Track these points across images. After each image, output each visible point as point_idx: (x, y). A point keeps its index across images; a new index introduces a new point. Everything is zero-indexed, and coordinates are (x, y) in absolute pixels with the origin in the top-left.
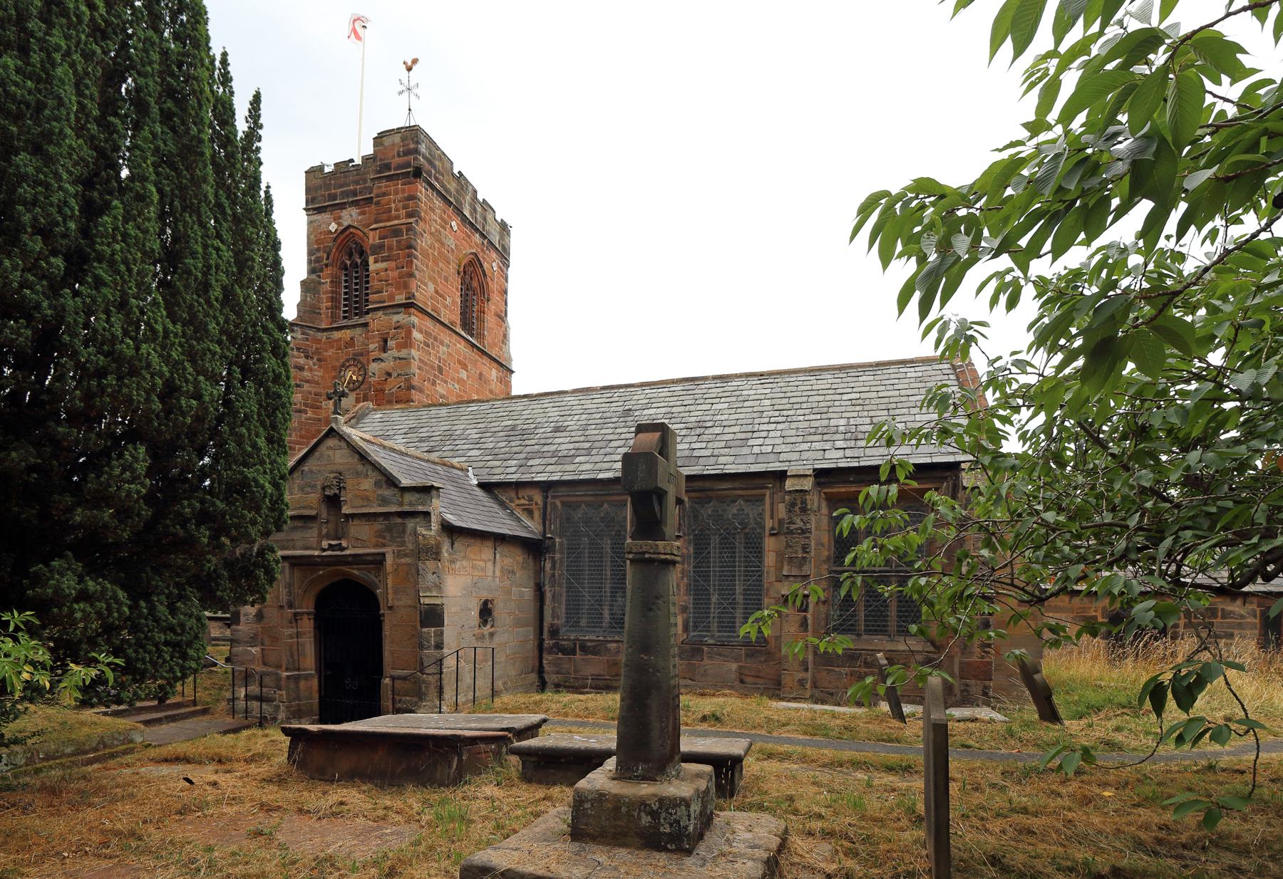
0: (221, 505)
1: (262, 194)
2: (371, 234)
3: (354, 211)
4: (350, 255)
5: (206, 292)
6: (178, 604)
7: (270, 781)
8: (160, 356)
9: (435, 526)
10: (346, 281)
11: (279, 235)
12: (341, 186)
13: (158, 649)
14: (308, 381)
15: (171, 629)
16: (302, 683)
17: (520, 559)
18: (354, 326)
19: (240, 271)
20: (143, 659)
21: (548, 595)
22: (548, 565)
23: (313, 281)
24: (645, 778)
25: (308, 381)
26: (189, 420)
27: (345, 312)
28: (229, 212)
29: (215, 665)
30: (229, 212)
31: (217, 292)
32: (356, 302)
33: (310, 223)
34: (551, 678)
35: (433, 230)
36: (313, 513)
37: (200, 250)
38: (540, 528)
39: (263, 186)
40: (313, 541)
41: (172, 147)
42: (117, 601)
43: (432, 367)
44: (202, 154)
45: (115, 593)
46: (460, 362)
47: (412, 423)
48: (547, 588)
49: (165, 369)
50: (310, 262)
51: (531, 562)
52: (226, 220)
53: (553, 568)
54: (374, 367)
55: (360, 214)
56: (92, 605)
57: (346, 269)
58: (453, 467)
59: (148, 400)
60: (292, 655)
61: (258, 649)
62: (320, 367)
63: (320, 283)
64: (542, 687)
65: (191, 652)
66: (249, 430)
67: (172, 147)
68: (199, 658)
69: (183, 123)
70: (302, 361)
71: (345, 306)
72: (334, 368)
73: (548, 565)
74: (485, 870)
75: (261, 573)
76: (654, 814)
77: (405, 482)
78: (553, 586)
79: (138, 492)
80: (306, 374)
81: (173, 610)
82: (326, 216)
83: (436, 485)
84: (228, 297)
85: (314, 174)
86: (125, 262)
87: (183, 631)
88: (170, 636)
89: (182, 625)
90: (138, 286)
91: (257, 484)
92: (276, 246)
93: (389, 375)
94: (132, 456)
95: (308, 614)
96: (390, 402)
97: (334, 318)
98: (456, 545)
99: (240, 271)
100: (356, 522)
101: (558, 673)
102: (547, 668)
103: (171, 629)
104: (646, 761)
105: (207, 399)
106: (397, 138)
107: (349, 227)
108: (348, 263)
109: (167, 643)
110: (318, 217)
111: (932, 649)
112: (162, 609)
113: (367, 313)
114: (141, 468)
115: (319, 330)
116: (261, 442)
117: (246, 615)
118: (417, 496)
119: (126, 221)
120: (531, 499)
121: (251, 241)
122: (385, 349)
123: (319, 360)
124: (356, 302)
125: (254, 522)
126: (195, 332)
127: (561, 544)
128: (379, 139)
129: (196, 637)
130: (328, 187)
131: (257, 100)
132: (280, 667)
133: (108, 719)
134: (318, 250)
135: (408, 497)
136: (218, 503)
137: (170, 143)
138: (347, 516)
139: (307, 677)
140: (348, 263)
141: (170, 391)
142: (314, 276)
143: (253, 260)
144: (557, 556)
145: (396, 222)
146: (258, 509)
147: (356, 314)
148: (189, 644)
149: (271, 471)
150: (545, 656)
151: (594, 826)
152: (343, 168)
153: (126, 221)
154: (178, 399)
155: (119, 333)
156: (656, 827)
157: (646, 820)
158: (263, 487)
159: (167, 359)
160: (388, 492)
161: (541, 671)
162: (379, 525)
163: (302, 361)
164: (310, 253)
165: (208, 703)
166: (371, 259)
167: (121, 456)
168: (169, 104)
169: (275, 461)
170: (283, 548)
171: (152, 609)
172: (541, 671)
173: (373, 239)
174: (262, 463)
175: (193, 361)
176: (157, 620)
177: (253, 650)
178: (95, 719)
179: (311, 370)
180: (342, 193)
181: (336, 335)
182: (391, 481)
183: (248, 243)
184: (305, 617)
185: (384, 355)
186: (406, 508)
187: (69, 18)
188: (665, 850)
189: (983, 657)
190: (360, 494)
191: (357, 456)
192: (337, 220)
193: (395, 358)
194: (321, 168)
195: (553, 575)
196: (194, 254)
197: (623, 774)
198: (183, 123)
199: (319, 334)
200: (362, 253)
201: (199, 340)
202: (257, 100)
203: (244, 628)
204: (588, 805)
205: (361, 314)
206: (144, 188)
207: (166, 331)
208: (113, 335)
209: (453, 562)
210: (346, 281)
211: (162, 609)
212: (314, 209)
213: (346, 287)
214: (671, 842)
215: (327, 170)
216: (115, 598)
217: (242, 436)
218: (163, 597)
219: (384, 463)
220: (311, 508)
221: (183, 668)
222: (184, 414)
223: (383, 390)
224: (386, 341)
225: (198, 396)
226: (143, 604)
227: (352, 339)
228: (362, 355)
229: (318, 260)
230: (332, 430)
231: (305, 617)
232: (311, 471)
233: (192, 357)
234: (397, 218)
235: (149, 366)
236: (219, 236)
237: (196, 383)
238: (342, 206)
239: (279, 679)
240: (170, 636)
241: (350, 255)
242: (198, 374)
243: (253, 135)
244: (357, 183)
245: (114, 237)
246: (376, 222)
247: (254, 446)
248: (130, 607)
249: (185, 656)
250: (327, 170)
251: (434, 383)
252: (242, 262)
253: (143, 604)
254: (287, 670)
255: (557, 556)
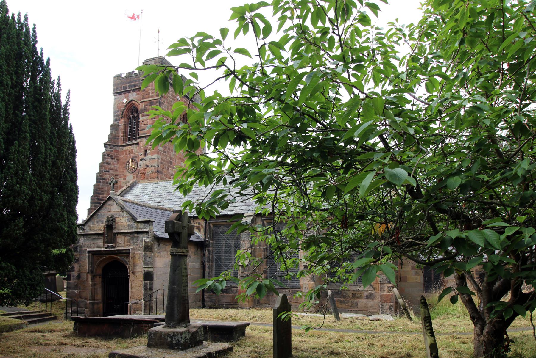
0: (48, 236)
1: (69, 126)
2: (141, 104)
3: (134, 93)
4: (132, 112)
5: (45, 164)
6: (33, 271)
7: (66, 336)
8: (29, 188)
9: (151, 237)
10: (130, 124)
11: (75, 139)
12: (129, 83)
13: (25, 286)
14: (112, 169)
15: (30, 279)
16: (96, 306)
17: (194, 250)
18: (133, 144)
19: (59, 154)
20: (20, 290)
21: (207, 266)
22: (207, 253)
23: (115, 125)
24: (172, 327)
25: (112, 169)
26: (38, 208)
27: (129, 138)
28: (56, 134)
29: (61, 298)
30: (56, 134)
31: (50, 163)
32: (134, 133)
33: (115, 99)
34: (208, 303)
35: (168, 101)
36: (102, 232)
37: (44, 151)
38: (204, 236)
39: (69, 124)
40: (102, 245)
41: (36, 117)
42: (12, 270)
43: (167, 162)
44: (46, 119)
45: (11, 267)
46: (180, 159)
47: (153, 189)
48: (206, 263)
49: (30, 192)
50: (114, 116)
51: (199, 252)
52: (55, 138)
53: (209, 254)
54: (140, 163)
55: (137, 95)
56: (3, 271)
57: (130, 119)
58: (166, 210)
59: (24, 203)
60: (92, 294)
61: (78, 291)
62: (118, 163)
63: (119, 125)
64: (204, 307)
65: (38, 288)
66: (59, 210)
67: (36, 117)
68: (41, 290)
69: (40, 109)
70: (110, 160)
71: (130, 135)
72: (124, 163)
73: (207, 253)
74: (115, 354)
75: (232, 243)
76: (171, 337)
77: (139, 220)
78: (209, 262)
79: (20, 233)
80: (111, 166)
81: (31, 272)
82: (122, 96)
83: (151, 220)
84: (54, 163)
85: (118, 77)
86: (18, 160)
87: (35, 280)
88: (30, 282)
89: (34, 278)
90: (22, 167)
91: (62, 228)
92: (74, 142)
93: (147, 166)
94: (18, 221)
95: (99, 275)
96: (147, 178)
97: (125, 141)
98: (161, 245)
99: (59, 154)
100: (119, 236)
101: (211, 302)
102: (206, 299)
103: (30, 279)
104: (173, 321)
105: (44, 200)
106: (152, 63)
107: (132, 100)
108: (131, 116)
109: (28, 285)
110: (119, 96)
111: (372, 289)
112: (27, 273)
113: (139, 138)
114: (21, 225)
115: (118, 146)
116: (65, 213)
117: (73, 276)
118: (144, 225)
119: (19, 146)
120: (199, 224)
121: (63, 144)
122: (145, 155)
123: (117, 160)
124: (134, 133)
125: (61, 241)
126: (41, 178)
127: (213, 243)
128: (145, 63)
129: (40, 283)
130: (123, 83)
131: (69, 92)
132: (86, 299)
133: (14, 320)
134: (118, 111)
135: (140, 225)
136: (48, 235)
137: (35, 117)
138: (116, 234)
139: (98, 303)
140: (131, 116)
141: (32, 198)
142: (116, 123)
143: (64, 150)
144: (211, 249)
145: (152, 99)
146: (62, 237)
147: (134, 139)
148: (37, 285)
149: (68, 223)
150: (205, 294)
151: (158, 342)
152: (130, 75)
153: (19, 146)
154: (35, 201)
155: (15, 182)
156: (172, 341)
157: (169, 339)
158: (64, 229)
159: (30, 189)
160: (132, 223)
161: (203, 301)
162: (127, 238)
163: (110, 160)
164: (115, 112)
165: (56, 315)
166: (140, 115)
167: (14, 221)
168: (36, 104)
169: (70, 219)
170: (90, 247)
171: (24, 272)
172: (203, 301)
173: (141, 106)
174: (64, 220)
175: (40, 188)
176: (25, 276)
177: (76, 291)
178: (9, 319)
179: (114, 164)
180: (129, 86)
181: (125, 148)
182: (134, 219)
183: (62, 145)
184: (98, 277)
185: (145, 158)
186: (139, 230)
187: (4, 86)
188: (174, 349)
189: (389, 292)
190: (123, 223)
191: (120, 208)
192: (127, 97)
193: (150, 159)
194: (120, 76)
195: (209, 257)
196: (41, 153)
197: (167, 326)
198: (40, 109)
199: (118, 148)
200: (137, 111)
201: (42, 181)
202: (69, 92)
203: (72, 281)
204: (152, 335)
205: (137, 139)
206: (25, 135)
207: (31, 180)
208: (13, 184)
209: (159, 252)
210: (130, 124)
211: (27, 273)
212: (117, 93)
213: (130, 127)
214: (176, 346)
215: (123, 76)
216: (11, 269)
217: (57, 212)
218: (27, 268)
219: (131, 211)
220: (101, 230)
221: (34, 294)
222: (36, 206)
223: (144, 173)
224: (146, 151)
225: (41, 199)
226: (21, 271)
227: (132, 150)
228: (136, 157)
229: (117, 116)
230: (110, 197)
231: (98, 277)
232: (102, 215)
233: (40, 186)
234: (152, 97)
235: (24, 192)
236: (52, 144)
237: (41, 196)
238: (129, 91)
239: (86, 304)
240: (30, 282)
241: (132, 112)
242: (42, 192)
243: (67, 105)
244: (136, 81)
245: (15, 153)
246: (143, 99)
247: (62, 214)
248: (16, 272)
249: (36, 290)
250: (123, 76)
251: (168, 169)
252: (60, 151)
253: (21, 271)
254: (90, 300)
255: (211, 249)
